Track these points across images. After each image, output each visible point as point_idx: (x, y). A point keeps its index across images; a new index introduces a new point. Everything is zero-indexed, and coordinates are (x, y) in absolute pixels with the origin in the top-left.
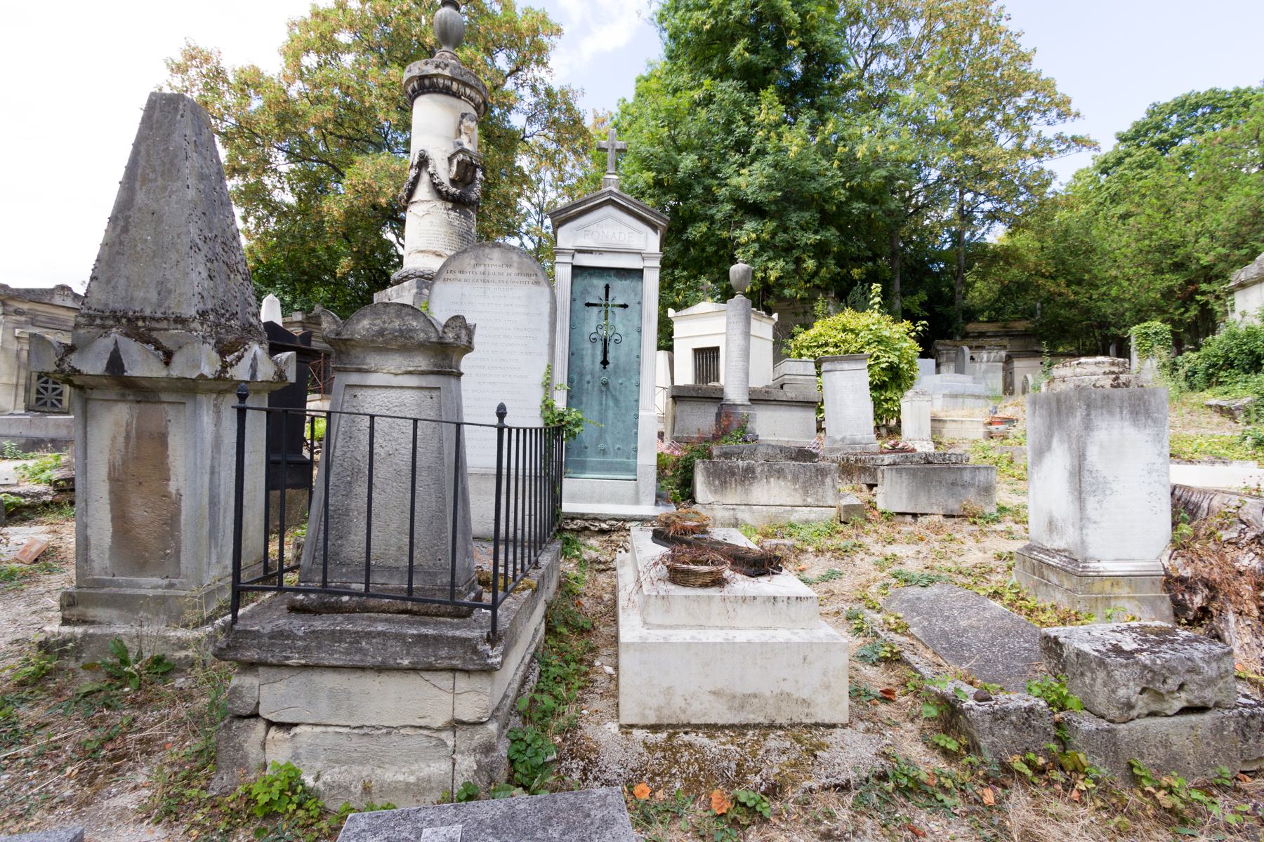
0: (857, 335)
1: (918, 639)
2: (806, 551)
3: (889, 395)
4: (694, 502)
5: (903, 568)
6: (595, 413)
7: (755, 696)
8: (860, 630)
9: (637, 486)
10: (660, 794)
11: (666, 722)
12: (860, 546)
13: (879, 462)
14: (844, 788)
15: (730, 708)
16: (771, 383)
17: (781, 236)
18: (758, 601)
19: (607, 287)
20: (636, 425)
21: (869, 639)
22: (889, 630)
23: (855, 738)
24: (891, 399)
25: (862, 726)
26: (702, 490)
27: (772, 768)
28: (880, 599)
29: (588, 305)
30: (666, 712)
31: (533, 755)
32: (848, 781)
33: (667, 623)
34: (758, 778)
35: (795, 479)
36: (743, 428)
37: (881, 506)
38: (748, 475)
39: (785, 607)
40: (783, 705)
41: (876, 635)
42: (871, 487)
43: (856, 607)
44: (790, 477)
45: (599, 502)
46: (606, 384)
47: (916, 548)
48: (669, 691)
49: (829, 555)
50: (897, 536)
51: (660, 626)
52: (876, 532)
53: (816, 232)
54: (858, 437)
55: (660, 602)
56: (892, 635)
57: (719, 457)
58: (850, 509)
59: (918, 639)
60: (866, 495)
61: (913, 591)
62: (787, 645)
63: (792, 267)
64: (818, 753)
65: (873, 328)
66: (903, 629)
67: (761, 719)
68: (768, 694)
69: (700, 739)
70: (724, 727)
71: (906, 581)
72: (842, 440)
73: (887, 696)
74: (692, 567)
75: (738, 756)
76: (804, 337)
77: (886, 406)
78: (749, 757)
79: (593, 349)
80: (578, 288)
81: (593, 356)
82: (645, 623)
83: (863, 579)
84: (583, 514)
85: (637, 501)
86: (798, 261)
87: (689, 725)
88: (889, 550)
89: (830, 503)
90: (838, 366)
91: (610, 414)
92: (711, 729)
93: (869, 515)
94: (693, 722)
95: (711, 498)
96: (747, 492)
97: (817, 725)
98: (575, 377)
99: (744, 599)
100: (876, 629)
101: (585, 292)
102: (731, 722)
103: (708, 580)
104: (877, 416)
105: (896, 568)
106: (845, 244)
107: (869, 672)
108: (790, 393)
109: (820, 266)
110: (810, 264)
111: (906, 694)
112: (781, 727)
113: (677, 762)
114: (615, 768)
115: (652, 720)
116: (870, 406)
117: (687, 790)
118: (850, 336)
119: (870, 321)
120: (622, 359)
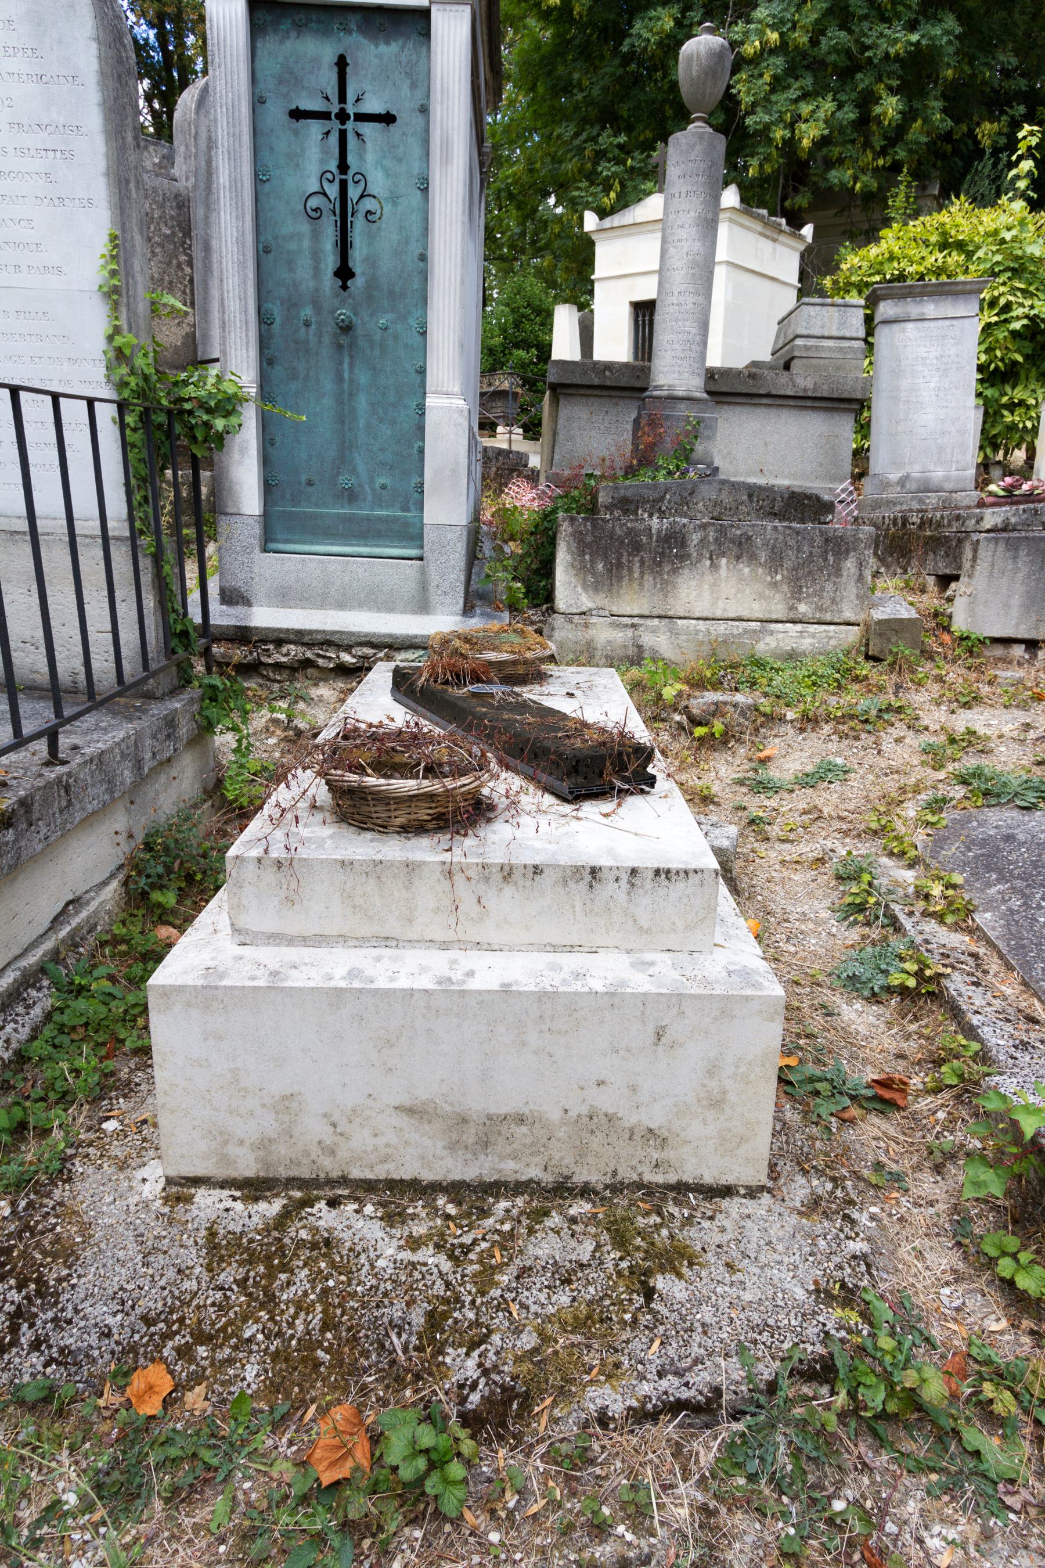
0: (969, 255)
1: (990, 943)
2: (782, 719)
3: (1019, 394)
4: (552, 610)
5: (984, 761)
6: (328, 402)
7: (521, 1120)
8: (861, 908)
9: (423, 572)
10: (196, 1399)
11: (283, 1173)
12: (899, 710)
13: (971, 524)
14: (703, 1410)
15: (453, 1147)
16: (766, 356)
17: (836, 36)
18: (548, 878)
19: (342, 63)
20: (421, 429)
21: (875, 934)
22: (925, 914)
23: (774, 1232)
24: (1022, 403)
25: (799, 1189)
26: (568, 588)
27: (518, 1331)
28: (920, 837)
29: (297, 114)
30: (282, 1150)
31: (5, 1218)
32: (717, 1391)
33: (295, 926)
34: (471, 1363)
35: (775, 561)
36: (686, 454)
37: (960, 624)
38: (669, 554)
39: (621, 896)
40: (595, 1142)
41: (895, 924)
42: (945, 581)
43: (864, 849)
44: (763, 556)
45: (341, 606)
46: (346, 328)
47: (1023, 717)
48: (287, 1104)
49: (827, 729)
50: (985, 689)
51: (275, 939)
52: (940, 679)
53: (912, 26)
54: (938, 474)
55: (270, 876)
56: (931, 926)
57: (609, 508)
58: (894, 627)
59: (990, 943)
60: (931, 600)
61: (999, 819)
62: (613, 999)
63: (849, 114)
64: (660, 1282)
65: (1008, 236)
66: (959, 915)
67: (533, 1173)
68: (555, 1115)
69: (357, 1225)
70: (436, 1188)
71: (986, 794)
72: (902, 482)
73: (885, 1096)
74: (372, 781)
75: (439, 1288)
76: (854, 261)
77: (1009, 418)
78: (467, 1292)
79: (316, 236)
80: (269, 66)
81: (316, 255)
82: (236, 930)
83: (891, 785)
84: (300, 633)
85: (423, 606)
86: (867, 100)
87: (344, 1181)
88: (962, 721)
89: (849, 615)
90: (912, 308)
91: (362, 403)
92: (394, 1196)
93: (931, 642)
94: (356, 1173)
95: (586, 602)
96: (666, 588)
97: (681, 1188)
98: (277, 311)
99: (507, 873)
100: (897, 908)
101: (290, 78)
102: (456, 1176)
103: (423, 814)
104: (989, 441)
105: (970, 762)
106: (972, 60)
107: (858, 1016)
108: (803, 380)
109: (908, 116)
110: (890, 107)
111: (936, 1091)
112: (586, 1191)
113: (270, 1301)
114: (101, 1312)
115: (248, 1167)
116: (972, 418)
117: (273, 1387)
118: (956, 258)
119: (1004, 219)
120: (386, 264)
